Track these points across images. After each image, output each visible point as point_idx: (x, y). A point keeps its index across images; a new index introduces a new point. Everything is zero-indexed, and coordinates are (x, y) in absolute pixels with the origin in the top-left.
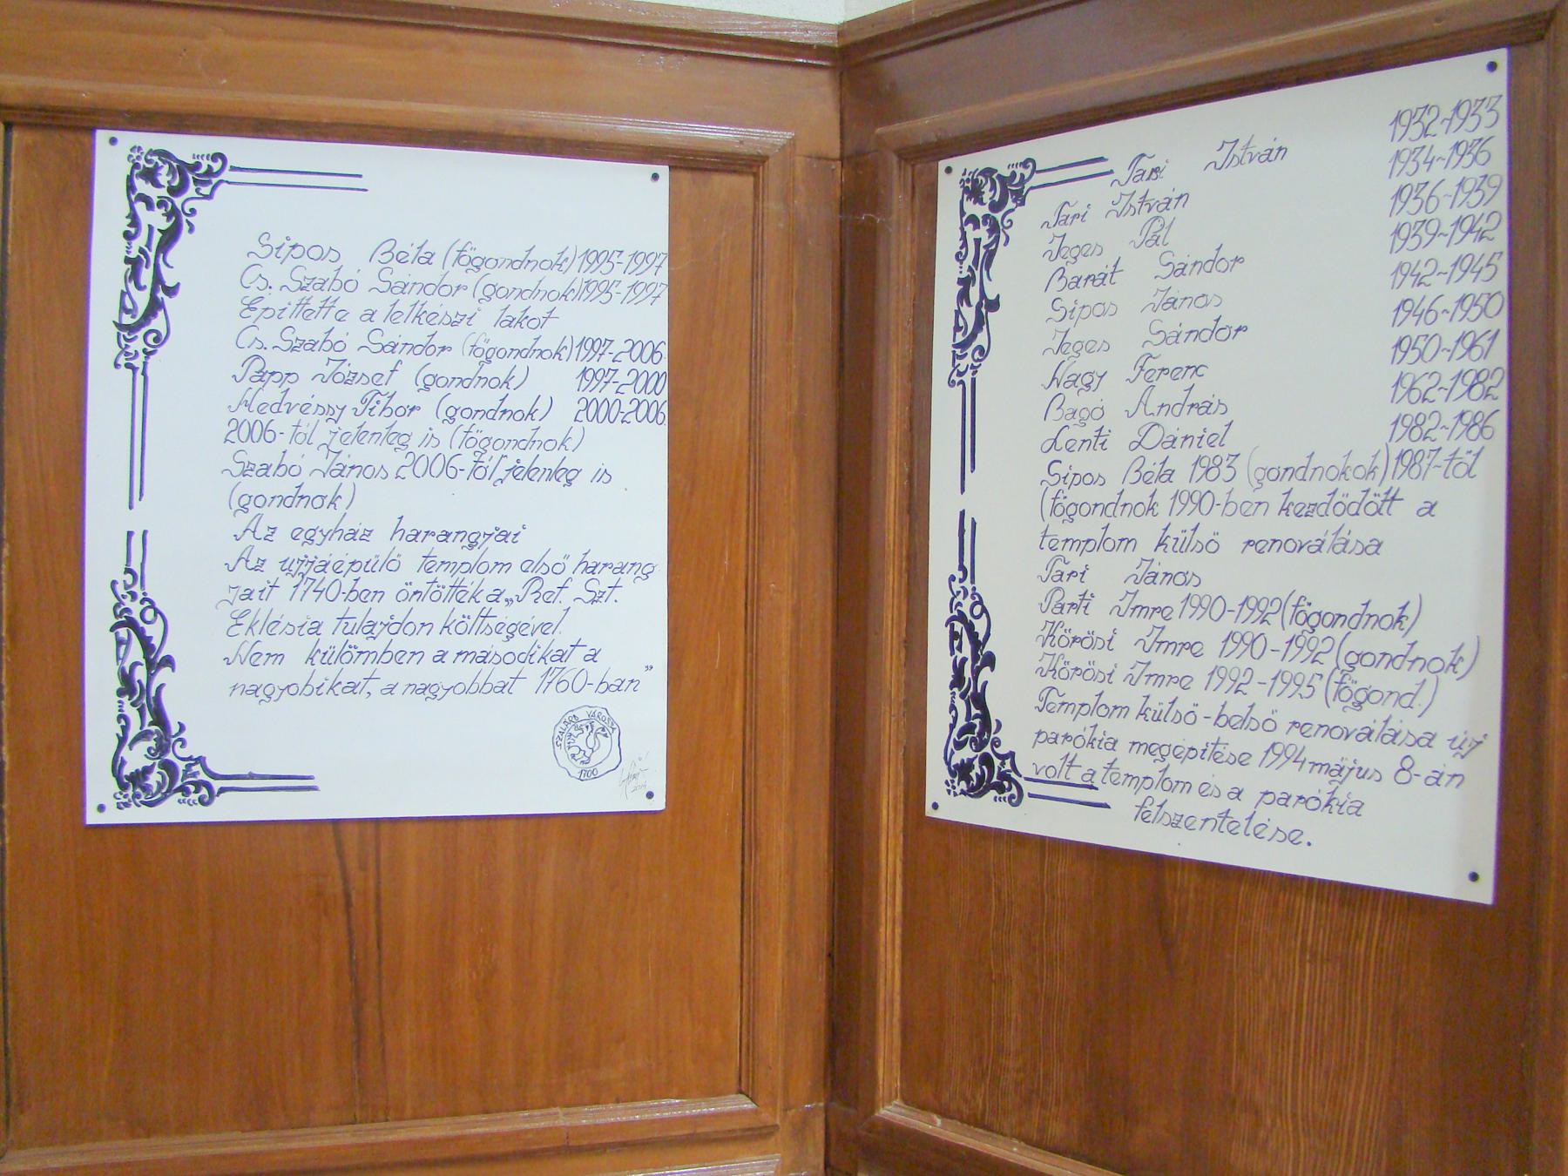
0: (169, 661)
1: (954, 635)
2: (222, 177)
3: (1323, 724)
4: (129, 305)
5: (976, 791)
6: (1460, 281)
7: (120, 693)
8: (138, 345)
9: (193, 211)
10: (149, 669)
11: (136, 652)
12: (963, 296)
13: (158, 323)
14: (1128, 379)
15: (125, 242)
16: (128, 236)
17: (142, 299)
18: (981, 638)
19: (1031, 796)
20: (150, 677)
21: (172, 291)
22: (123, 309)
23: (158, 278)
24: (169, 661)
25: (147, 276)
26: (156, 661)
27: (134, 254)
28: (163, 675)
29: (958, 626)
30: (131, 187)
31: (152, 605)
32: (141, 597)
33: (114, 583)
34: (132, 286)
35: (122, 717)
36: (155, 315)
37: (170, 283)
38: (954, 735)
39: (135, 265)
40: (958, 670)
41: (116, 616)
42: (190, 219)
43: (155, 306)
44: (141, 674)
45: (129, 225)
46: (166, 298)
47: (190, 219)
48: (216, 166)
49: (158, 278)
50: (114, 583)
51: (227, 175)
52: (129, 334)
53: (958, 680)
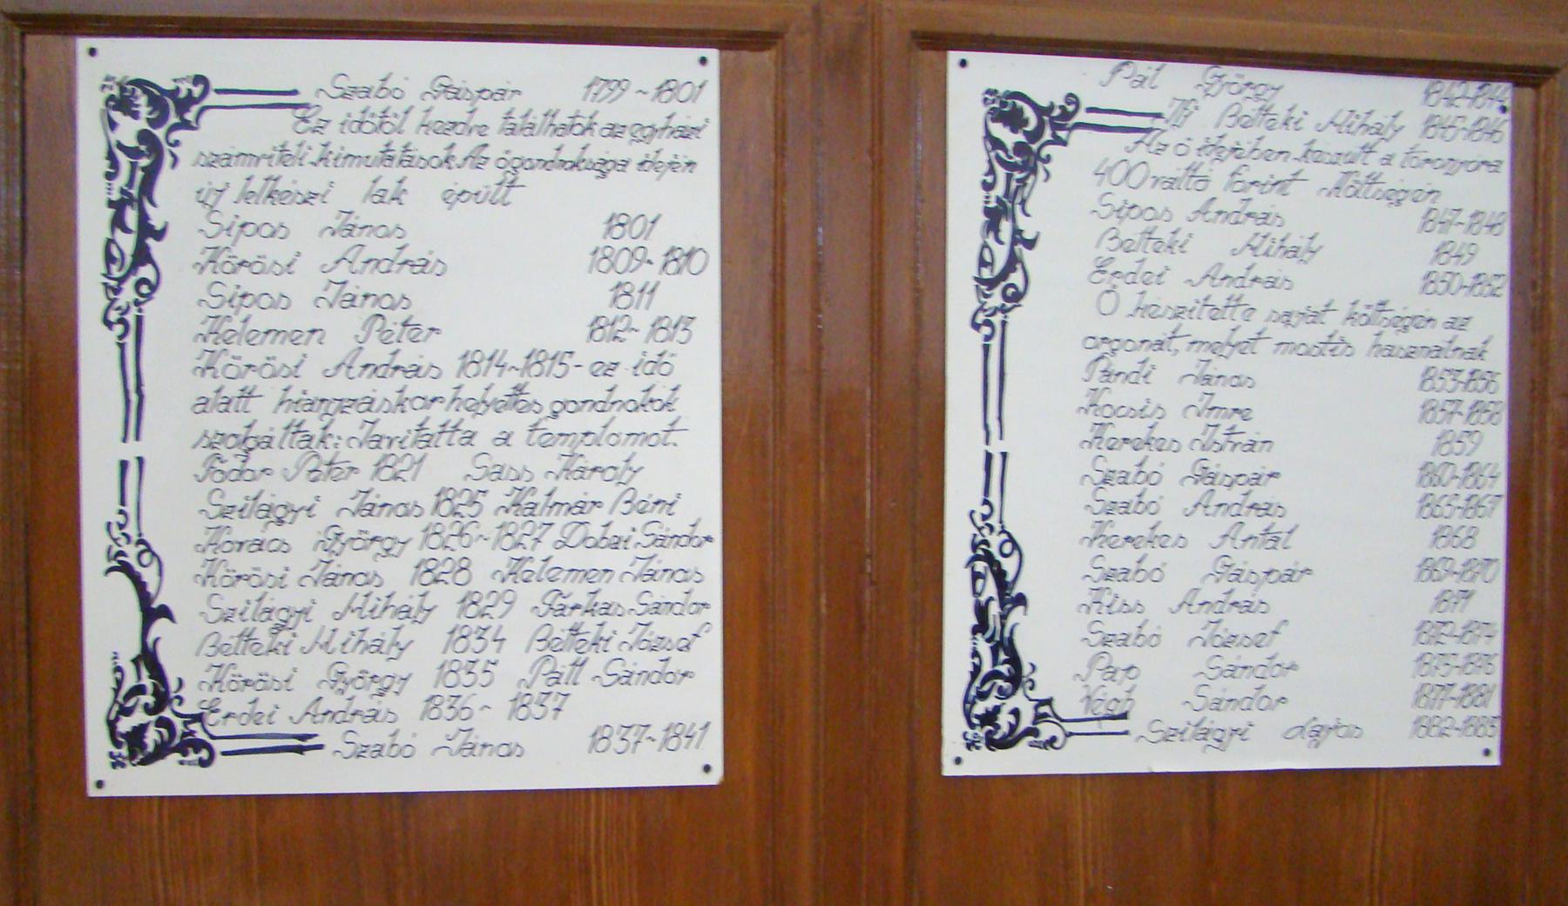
0: (1021, 600)
1: (976, 576)
2: (206, 102)
3: (626, 686)
4: (987, 258)
5: (1007, 743)
6: (615, 103)
7: (975, 630)
8: (996, 300)
9: (1048, 159)
10: (1002, 606)
11: (990, 589)
12: (118, 222)
13: (1016, 278)
14: (1190, 280)
15: (984, 193)
16: (988, 187)
17: (1001, 255)
18: (1009, 578)
19: (225, 753)
20: (1004, 617)
21: (1030, 244)
22: (982, 263)
23: (1017, 232)
24: (1021, 600)
25: (131, 217)
26: (1012, 599)
27: (116, 196)
28: (1016, 615)
29: (980, 566)
30: (988, 136)
31: (149, 549)
32: (135, 538)
33: (109, 524)
34: (991, 241)
35: (975, 654)
36: (1014, 270)
37: (1028, 235)
38: (977, 683)
39: (118, 207)
40: (981, 611)
41: (109, 560)
42: (174, 150)
43: (1013, 262)
44: (994, 609)
45: (986, 175)
46: (1025, 251)
47: (174, 150)
48: (197, 91)
49: (143, 218)
50: (109, 524)
51: (212, 99)
52: (988, 290)
53: (981, 627)
